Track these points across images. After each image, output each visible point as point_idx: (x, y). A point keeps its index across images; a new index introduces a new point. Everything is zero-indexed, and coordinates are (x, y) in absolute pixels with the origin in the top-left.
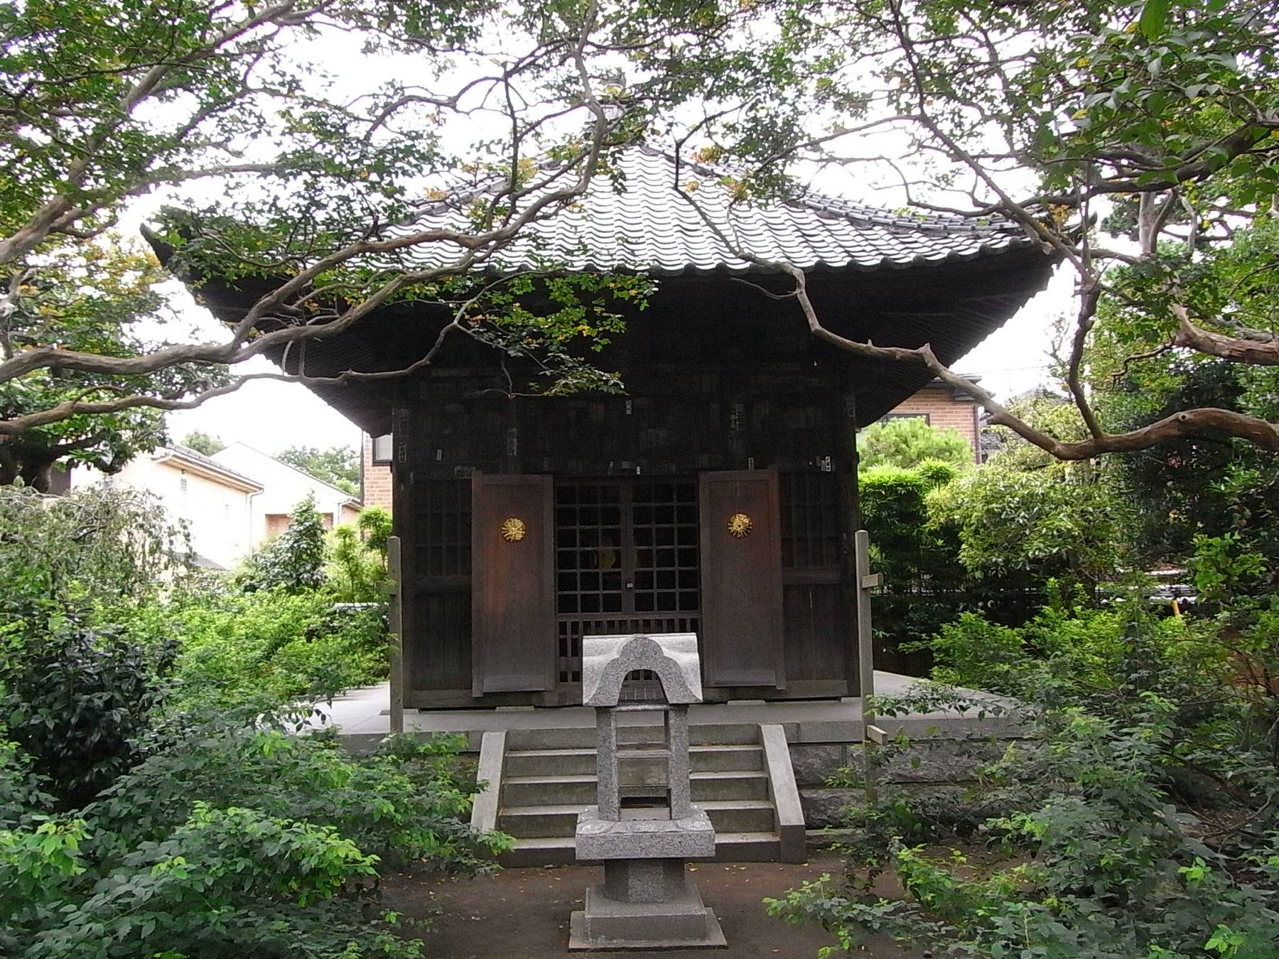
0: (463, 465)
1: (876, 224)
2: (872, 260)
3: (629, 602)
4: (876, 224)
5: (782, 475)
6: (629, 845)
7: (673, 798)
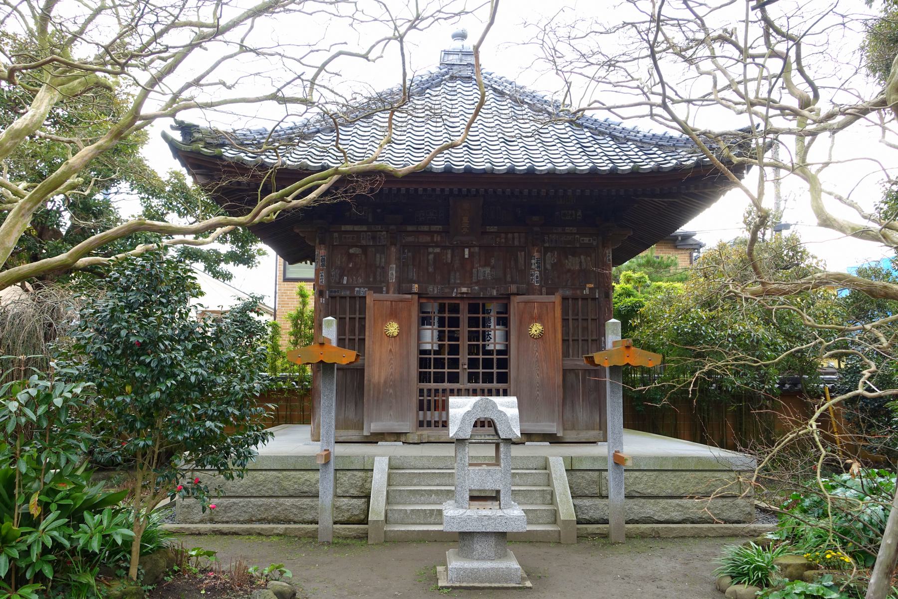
0: (360, 287)
1: (628, 140)
2: (626, 167)
3: (463, 377)
4: (628, 140)
5: (565, 299)
6: (475, 523)
7: (502, 495)
